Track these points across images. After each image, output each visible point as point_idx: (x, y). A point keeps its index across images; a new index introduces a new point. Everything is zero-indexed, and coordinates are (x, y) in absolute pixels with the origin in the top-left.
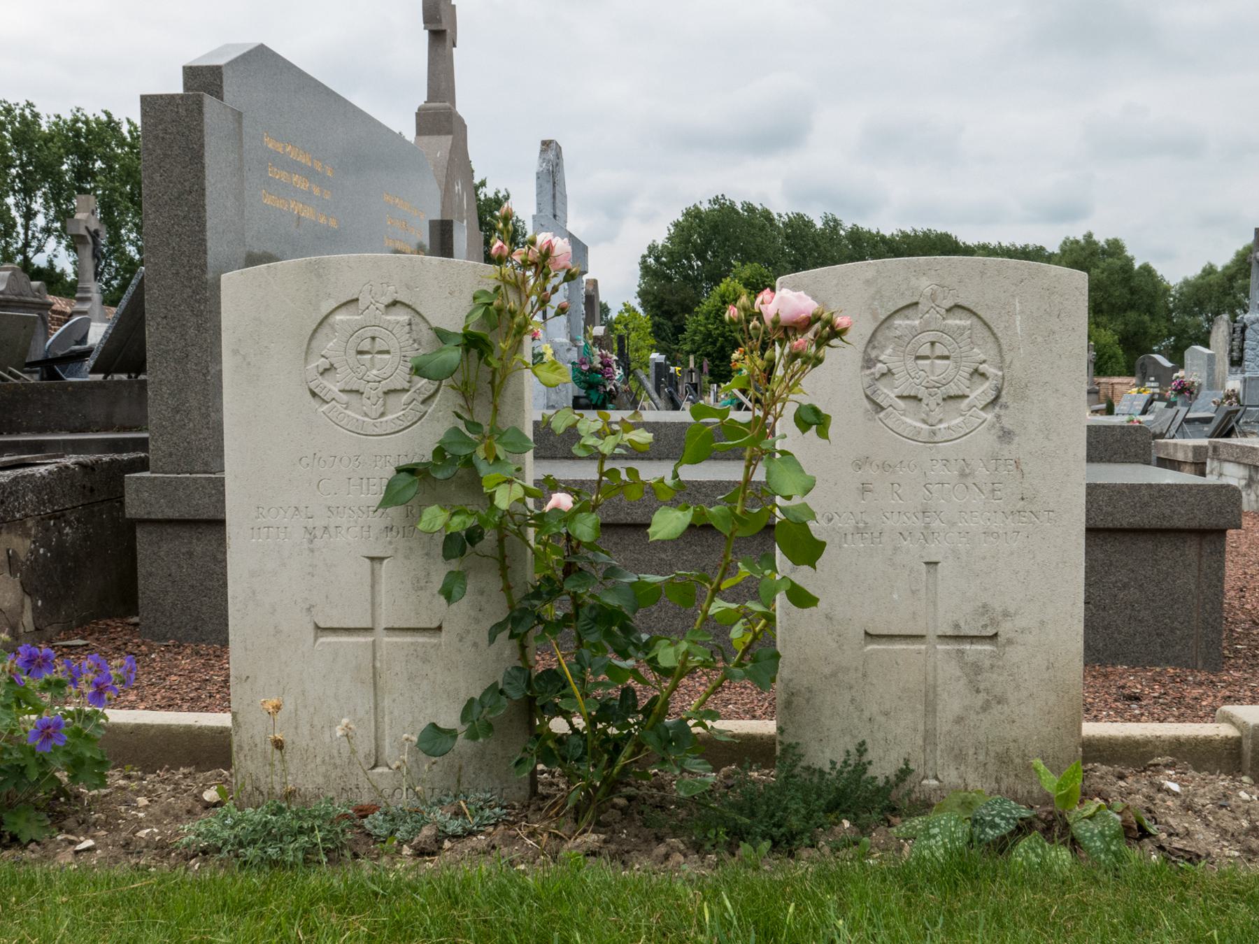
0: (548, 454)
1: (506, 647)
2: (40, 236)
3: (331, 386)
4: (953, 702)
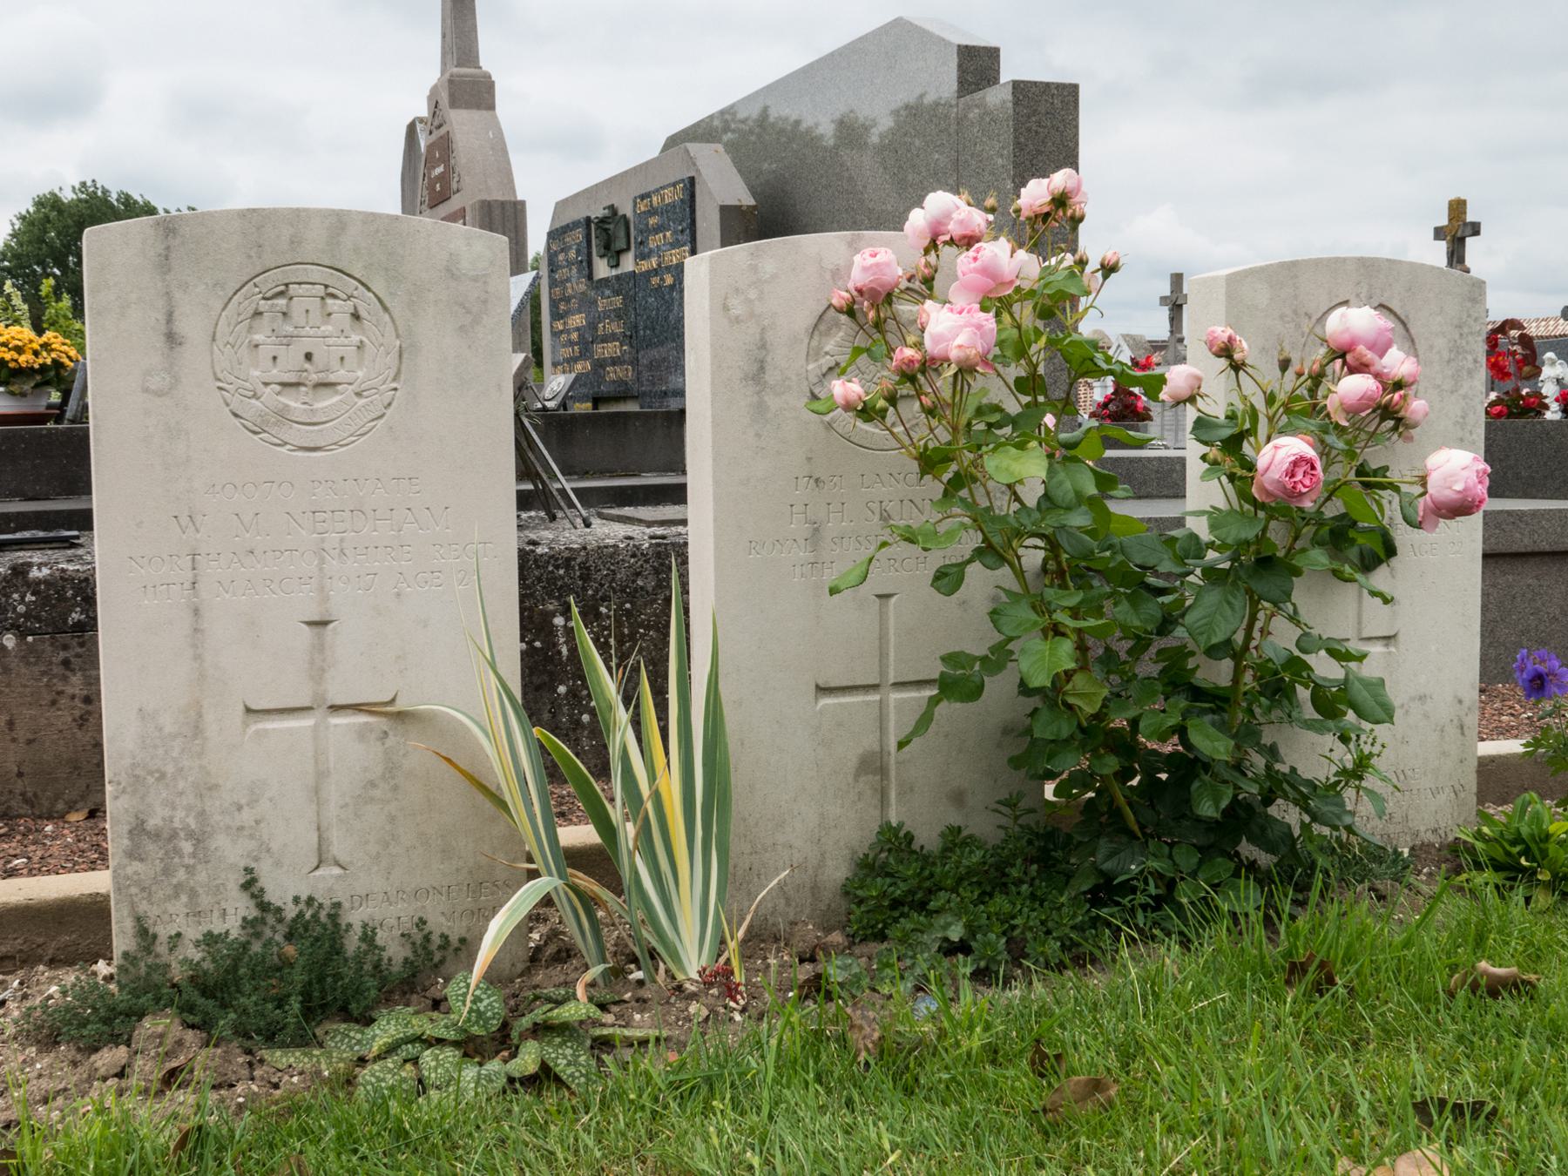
0: (1171, 492)
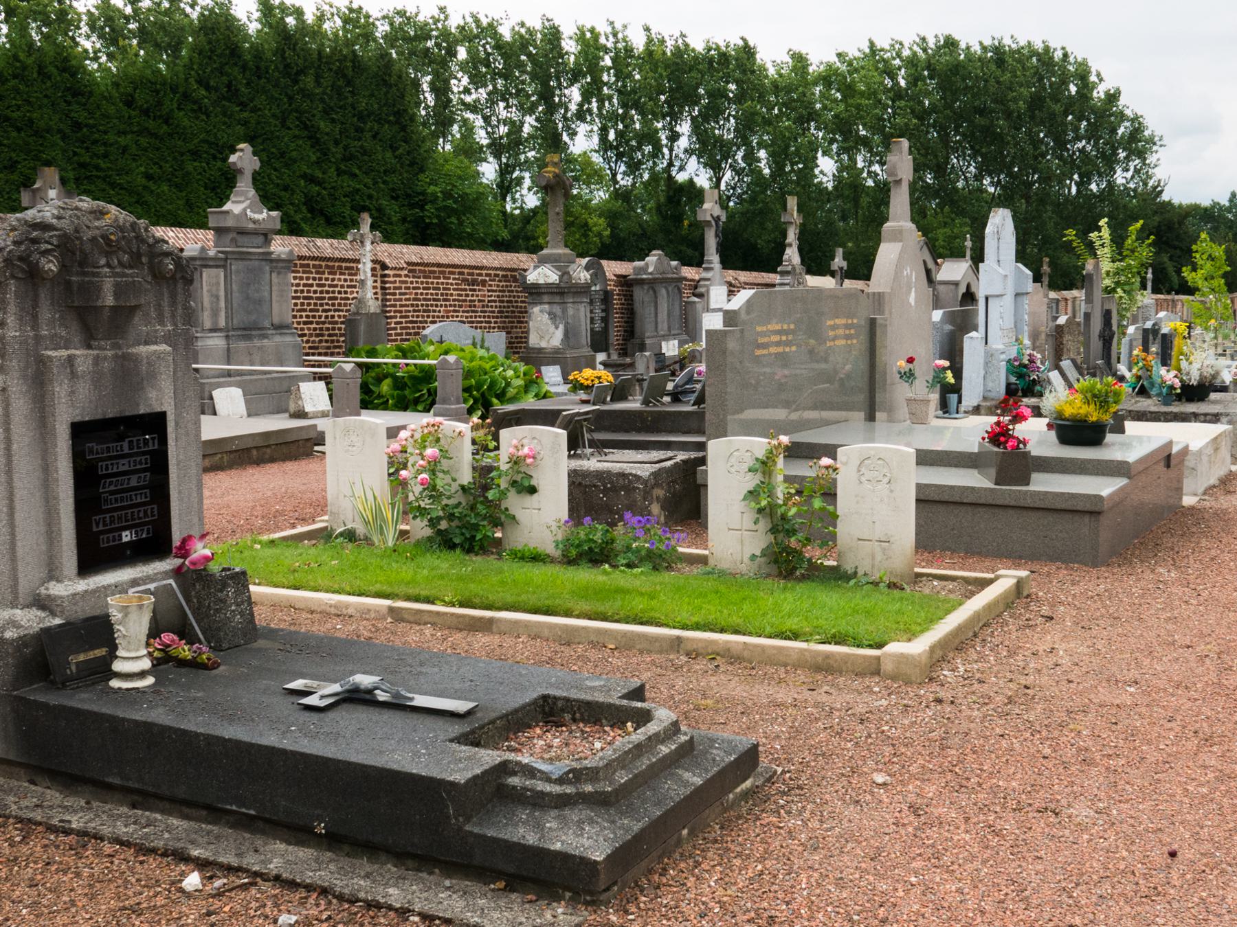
1: (771, 538)
2: (683, 156)
3: (733, 470)
4: (879, 557)
